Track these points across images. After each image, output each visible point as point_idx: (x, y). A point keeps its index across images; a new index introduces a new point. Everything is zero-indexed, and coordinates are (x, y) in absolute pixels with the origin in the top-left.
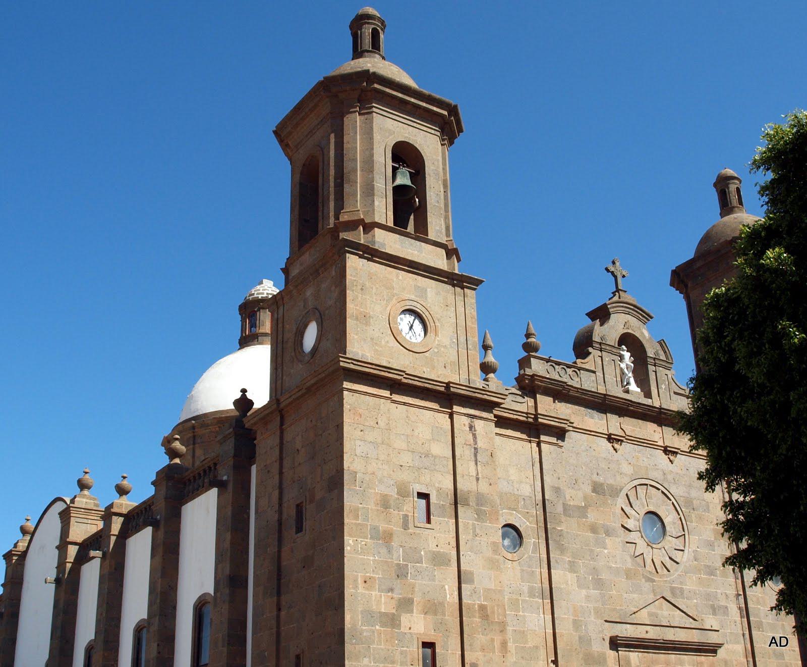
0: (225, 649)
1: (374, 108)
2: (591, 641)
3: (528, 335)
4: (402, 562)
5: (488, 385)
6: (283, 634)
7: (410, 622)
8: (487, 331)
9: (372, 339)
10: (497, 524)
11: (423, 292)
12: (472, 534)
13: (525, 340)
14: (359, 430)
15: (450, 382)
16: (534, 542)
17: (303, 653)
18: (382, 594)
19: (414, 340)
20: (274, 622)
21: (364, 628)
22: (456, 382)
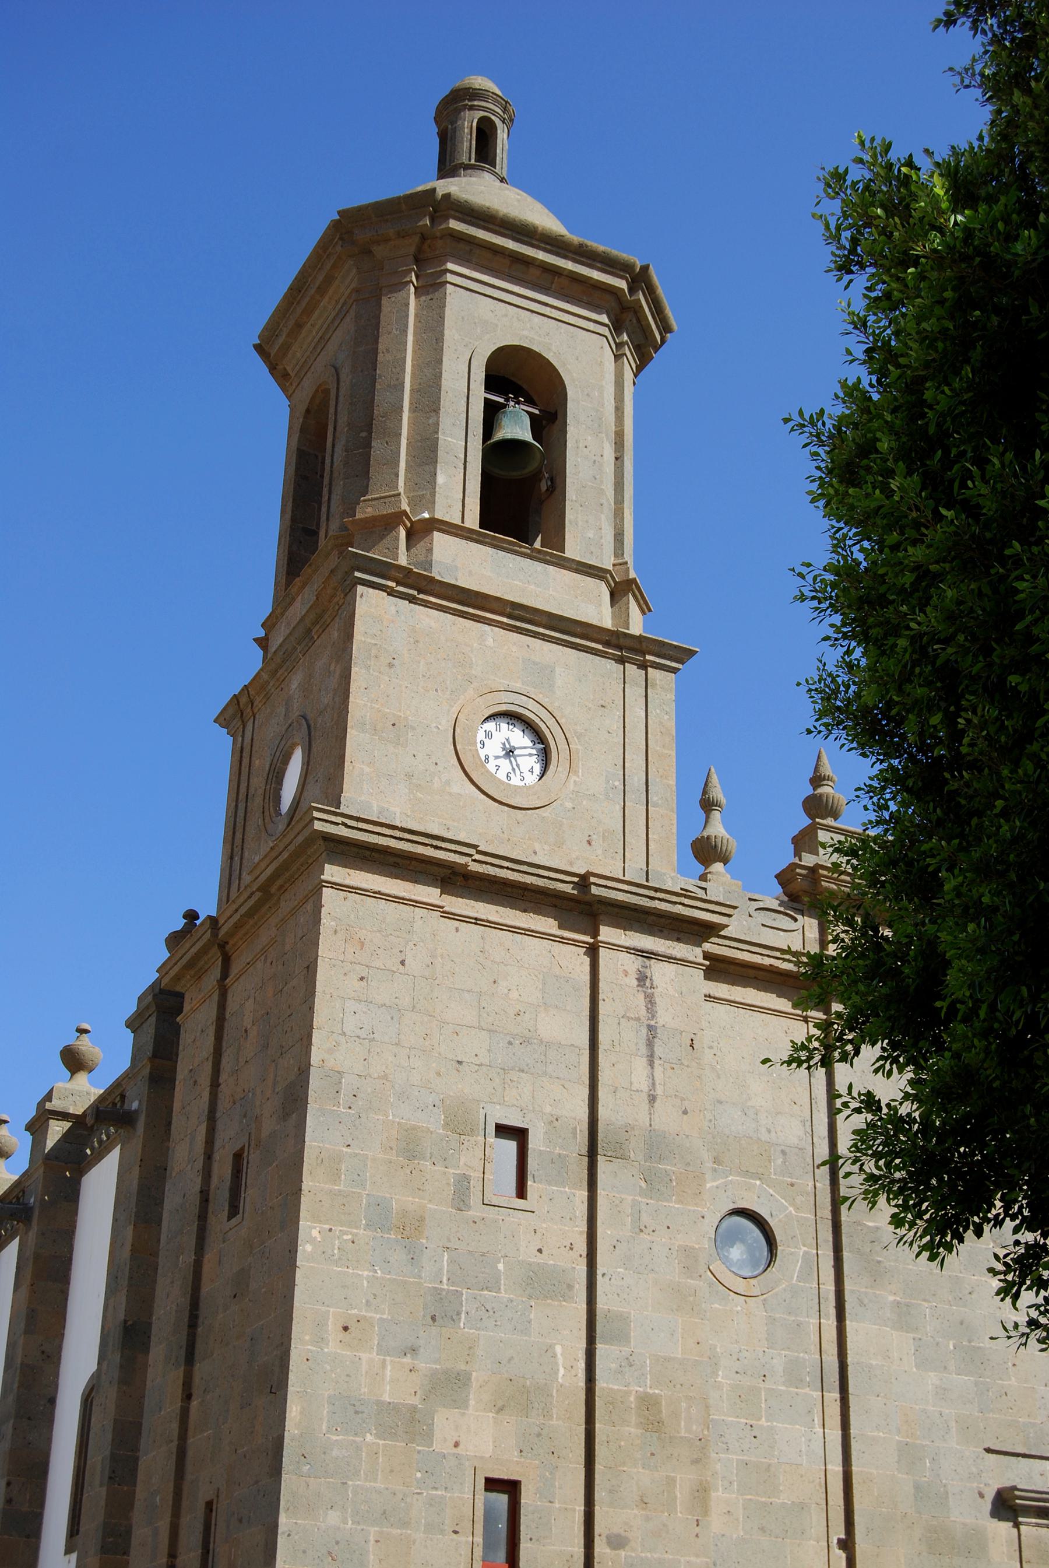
0: (104, 1491)
1: (448, 274)
2: (947, 1498)
3: (817, 780)
4: (446, 1287)
8: (713, 770)
9: (409, 776)
12: (630, 1228)
13: (809, 791)
14: (356, 977)
15: (589, 874)
16: (805, 1253)
18: (388, 1358)
21: (335, 1438)
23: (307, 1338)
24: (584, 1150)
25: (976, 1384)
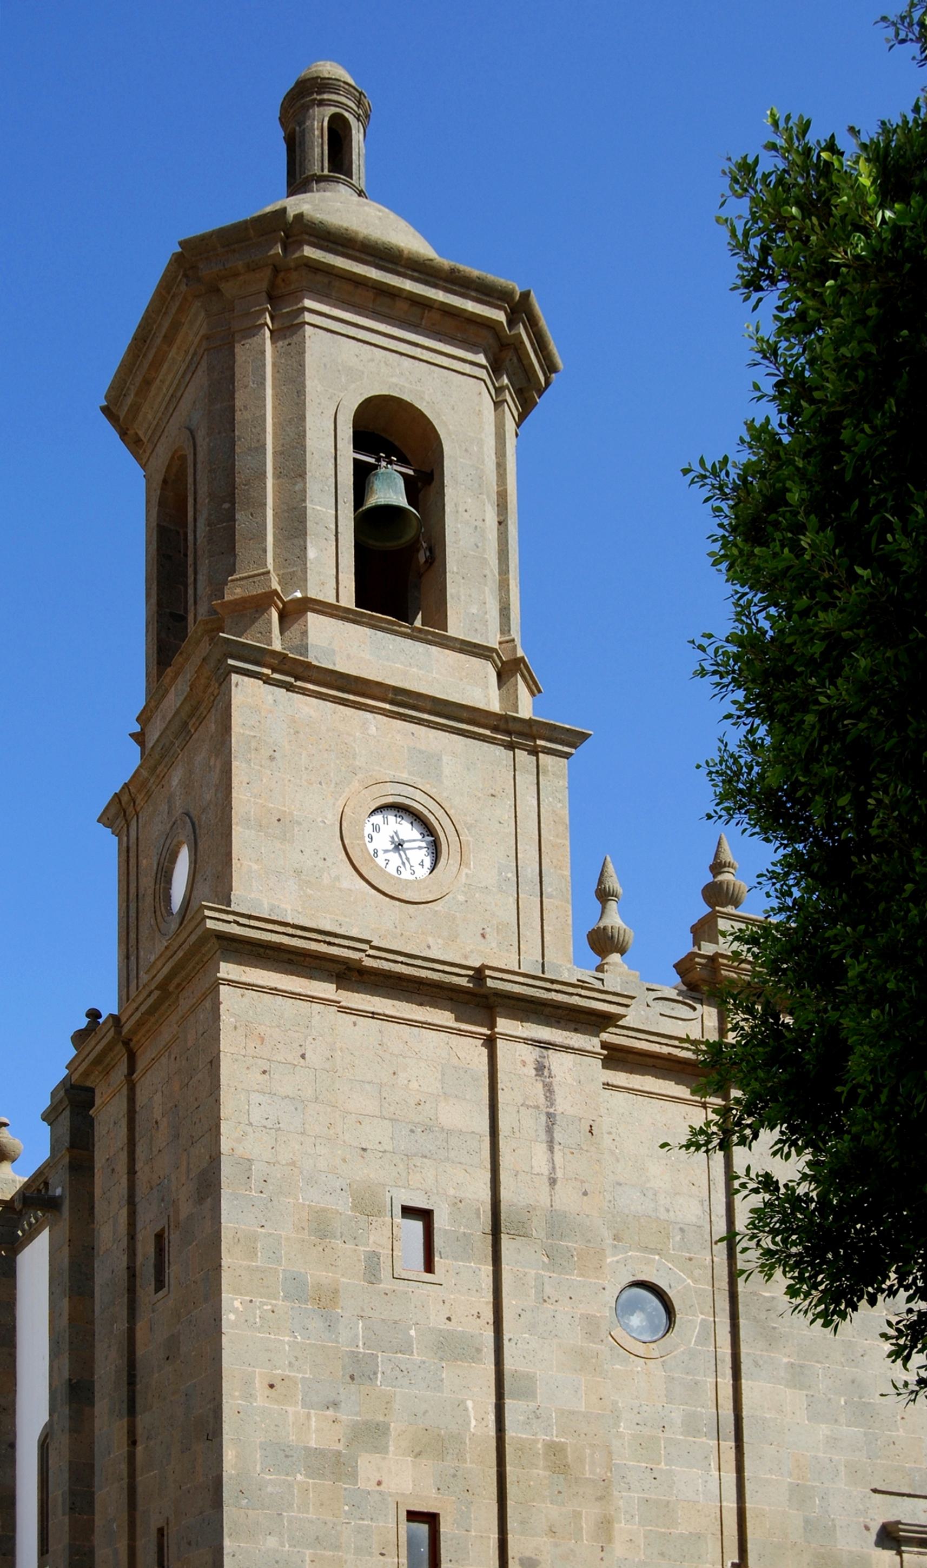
0: (66, 1519)
1: (306, 313)
3: (718, 867)
4: (362, 1350)
5: (602, 980)
6: (140, 1489)
7: (379, 1469)
8: (609, 859)
9: (298, 872)
10: (597, 1278)
11: (431, 763)
13: (709, 878)
17: (168, 1524)
18: (312, 1411)
19: (406, 875)
20: (124, 1467)
21: (268, 1477)
22: (512, 969)
23: (237, 1394)
24: (488, 1229)
25: (865, 1434)
